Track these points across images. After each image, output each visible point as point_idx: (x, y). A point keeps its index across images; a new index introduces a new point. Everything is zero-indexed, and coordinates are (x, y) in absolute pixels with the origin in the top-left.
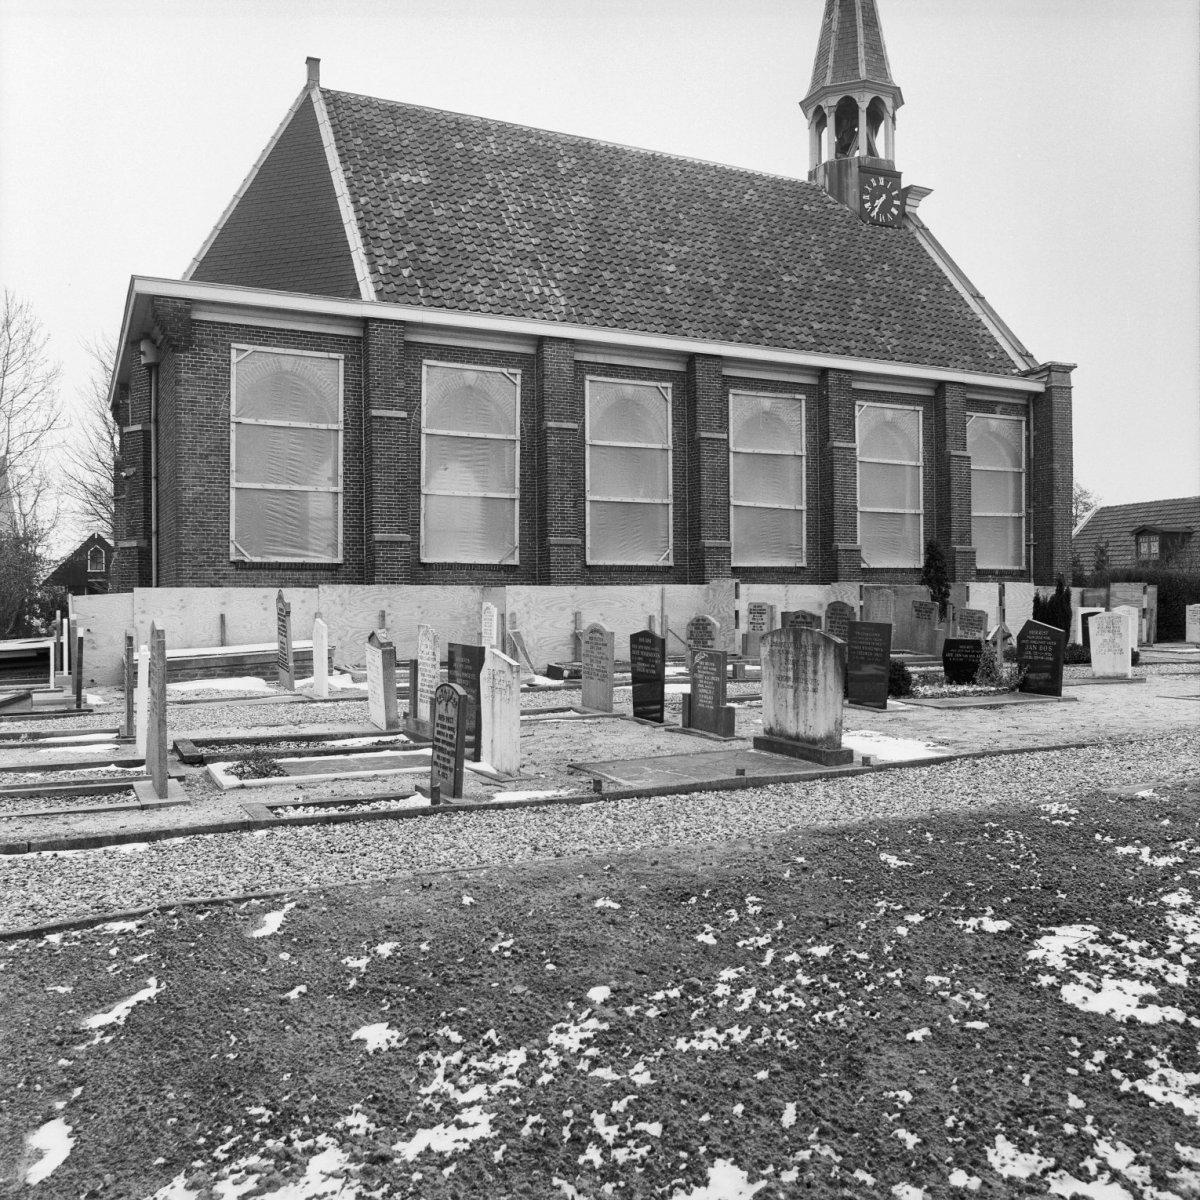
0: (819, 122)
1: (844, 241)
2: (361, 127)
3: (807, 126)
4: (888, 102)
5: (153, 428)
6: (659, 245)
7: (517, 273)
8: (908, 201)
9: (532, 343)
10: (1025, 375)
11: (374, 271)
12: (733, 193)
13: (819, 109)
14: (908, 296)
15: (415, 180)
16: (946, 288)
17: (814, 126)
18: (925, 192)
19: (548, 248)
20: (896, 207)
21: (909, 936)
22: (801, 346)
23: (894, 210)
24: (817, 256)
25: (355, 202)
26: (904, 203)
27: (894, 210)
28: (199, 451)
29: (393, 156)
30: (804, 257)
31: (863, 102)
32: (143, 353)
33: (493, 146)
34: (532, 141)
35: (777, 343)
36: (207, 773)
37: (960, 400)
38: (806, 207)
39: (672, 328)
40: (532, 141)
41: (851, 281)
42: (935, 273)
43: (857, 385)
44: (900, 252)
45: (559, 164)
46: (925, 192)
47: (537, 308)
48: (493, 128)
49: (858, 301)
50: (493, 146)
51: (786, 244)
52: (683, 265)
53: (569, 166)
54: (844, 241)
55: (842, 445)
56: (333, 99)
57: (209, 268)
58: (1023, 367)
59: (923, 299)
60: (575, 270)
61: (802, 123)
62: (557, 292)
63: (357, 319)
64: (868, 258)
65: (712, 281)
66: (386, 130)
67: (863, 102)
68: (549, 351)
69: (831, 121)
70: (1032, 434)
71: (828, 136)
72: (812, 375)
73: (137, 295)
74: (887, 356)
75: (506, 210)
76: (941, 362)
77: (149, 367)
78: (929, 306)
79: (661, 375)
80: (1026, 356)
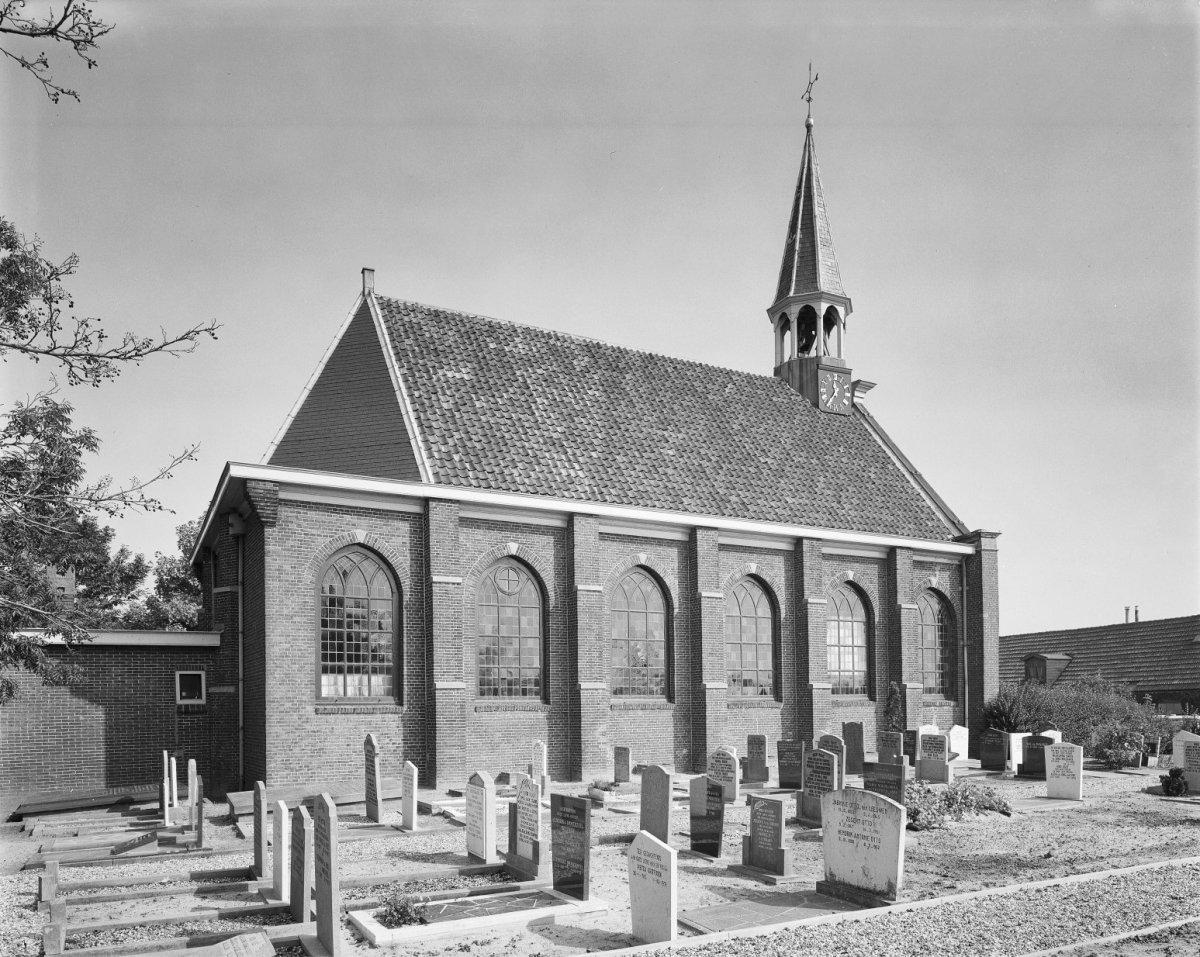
0: (783, 325)
1: (807, 428)
2: (413, 329)
3: (772, 330)
4: (841, 310)
5: (240, 590)
6: (660, 432)
7: (549, 456)
8: (856, 394)
9: (789, 540)
10: (957, 540)
11: (431, 456)
12: (717, 387)
13: (784, 315)
14: (860, 473)
15: (458, 375)
16: (890, 467)
17: (779, 330)
18: (869, 386)
19: (570, 434)
20: (848, 398)
21: (222, 621)
22: (779, 519)
23: (845, 401)
24: (786, 440)
25: (411, 396)
26: (853, 395)
27: (845, 401)
28: (285, 612)
29: (438, 353)
30: (776, 441)
31: (822, 308)
32: (231, 525)
33: (520, 346)
34: (552, 342)
35: (759, 517)
36: (343, 886)
37: (908, 561)
38: (774, 399)
39: (677, 506)
40: (552, 342)
41: (814, 461)
42: (880, 454)
43: (282, 495)
44: (852, 436)
45: (575, 362)
46: (869, 386)
47: (566, 488)
48: (519, 331)
49: (822, 479)
50: (520, 346)
51: (761, 430)
52: (681, 450)
53: (583, 364)
54: (807, 428)
55: (815, 601)
56: (387, 305)
57: (285, 455)
58: (957, 534)
59: (873, 476)
60: (594, 454)
61: (769, 328)
62: (580, 473)
63: (419, 498)
64: (827, 442)
65: (705, 463)
66: (430, 331)
67: (822, 308)
68: (578, 523)
69: (794, 326)
70: (965, 588)
71: (791, 338)
72: (882, 552)
73: (232, 478)
74: (848, 526)
75: (535, 402)
76: (891, 529)
77: (236, 537)
78: (878, 482)
79: (403, 516)
80: (955, 523)
